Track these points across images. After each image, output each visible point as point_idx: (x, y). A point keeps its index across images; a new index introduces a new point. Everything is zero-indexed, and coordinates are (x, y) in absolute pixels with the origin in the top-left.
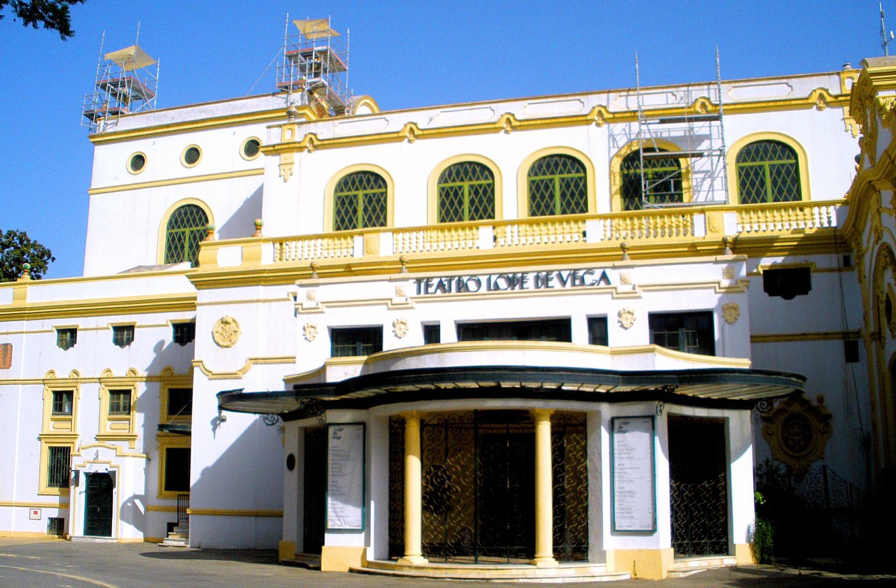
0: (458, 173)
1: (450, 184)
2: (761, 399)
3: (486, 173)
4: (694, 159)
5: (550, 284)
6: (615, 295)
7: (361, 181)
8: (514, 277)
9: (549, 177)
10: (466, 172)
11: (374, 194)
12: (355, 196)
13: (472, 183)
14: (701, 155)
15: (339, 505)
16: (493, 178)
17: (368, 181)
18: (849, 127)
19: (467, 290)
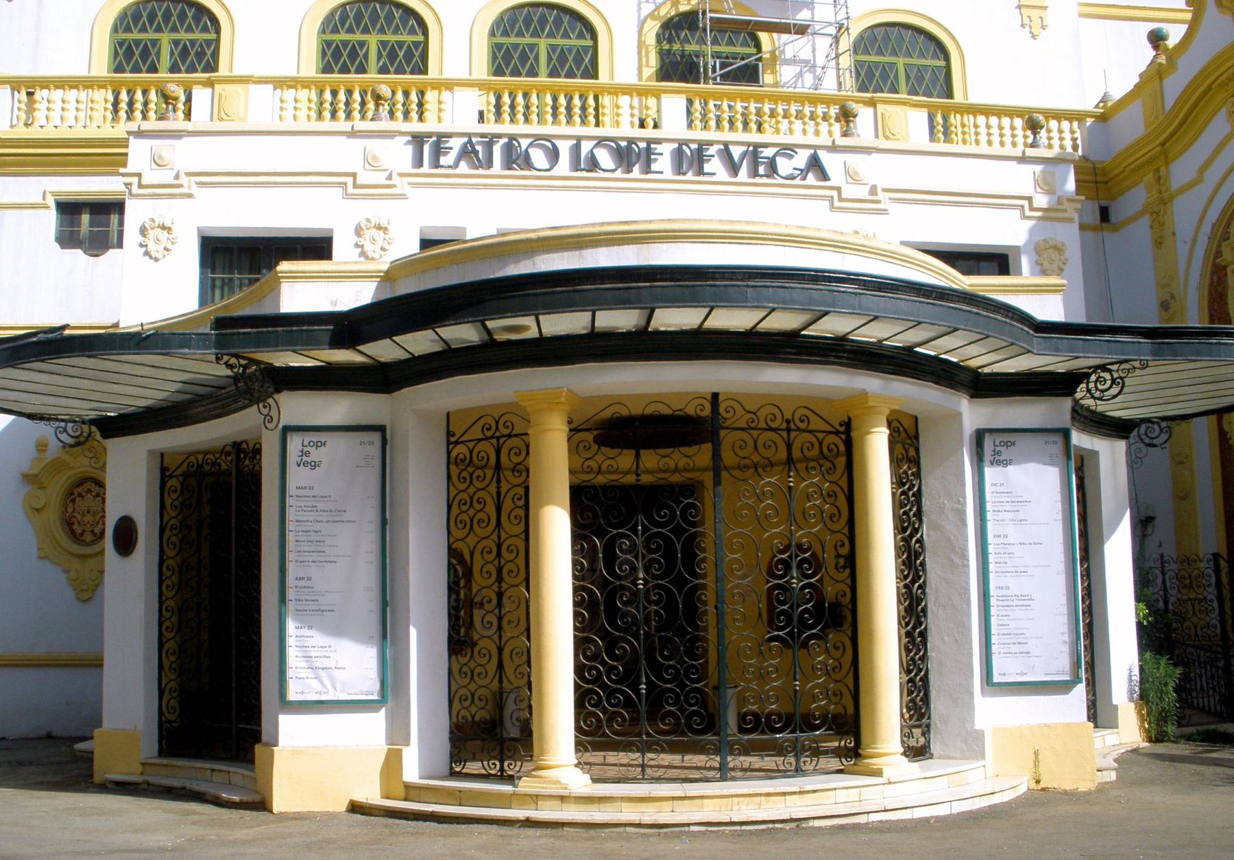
2: (1148, 420)
3: (412, 22)
4: (785, 37)
5: (707, 168)
8: (629, 147)
9: (528, 40)
13: (385, 38)
14: (801, 30)
15: (317, 639)
18: (1026, 21)
19: (527, 163)
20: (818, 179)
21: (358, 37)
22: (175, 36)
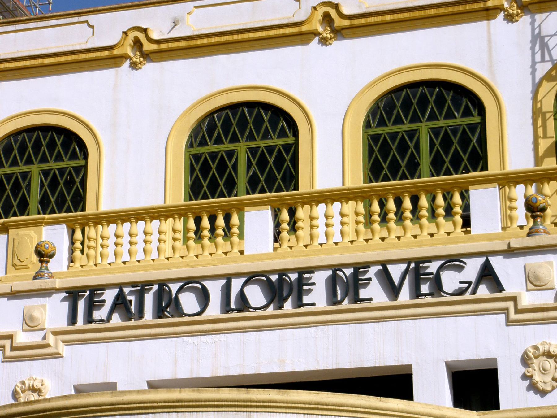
0: (227, 125)
1: (212, 148)
3: (283, 123)
5: (363, 293)
6: (513, 316)
7: (37, 146)
9: (408, 126)
10: (243, 123)
11: (62, 171)
12: (25, 175)
13: (253, 144)
16: (296, 134)
17: (52, 145)
19: (179, 311)
20: (492, 290)
21: (227, 146)
22: (45, 166)
